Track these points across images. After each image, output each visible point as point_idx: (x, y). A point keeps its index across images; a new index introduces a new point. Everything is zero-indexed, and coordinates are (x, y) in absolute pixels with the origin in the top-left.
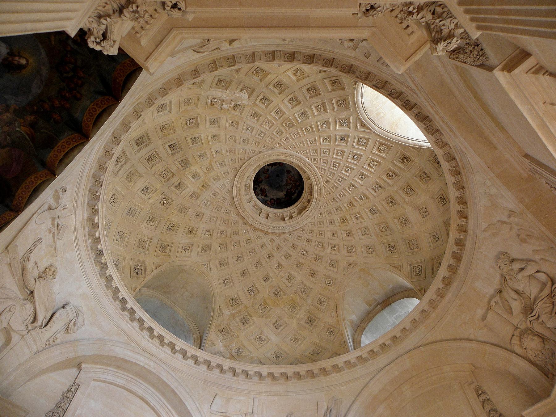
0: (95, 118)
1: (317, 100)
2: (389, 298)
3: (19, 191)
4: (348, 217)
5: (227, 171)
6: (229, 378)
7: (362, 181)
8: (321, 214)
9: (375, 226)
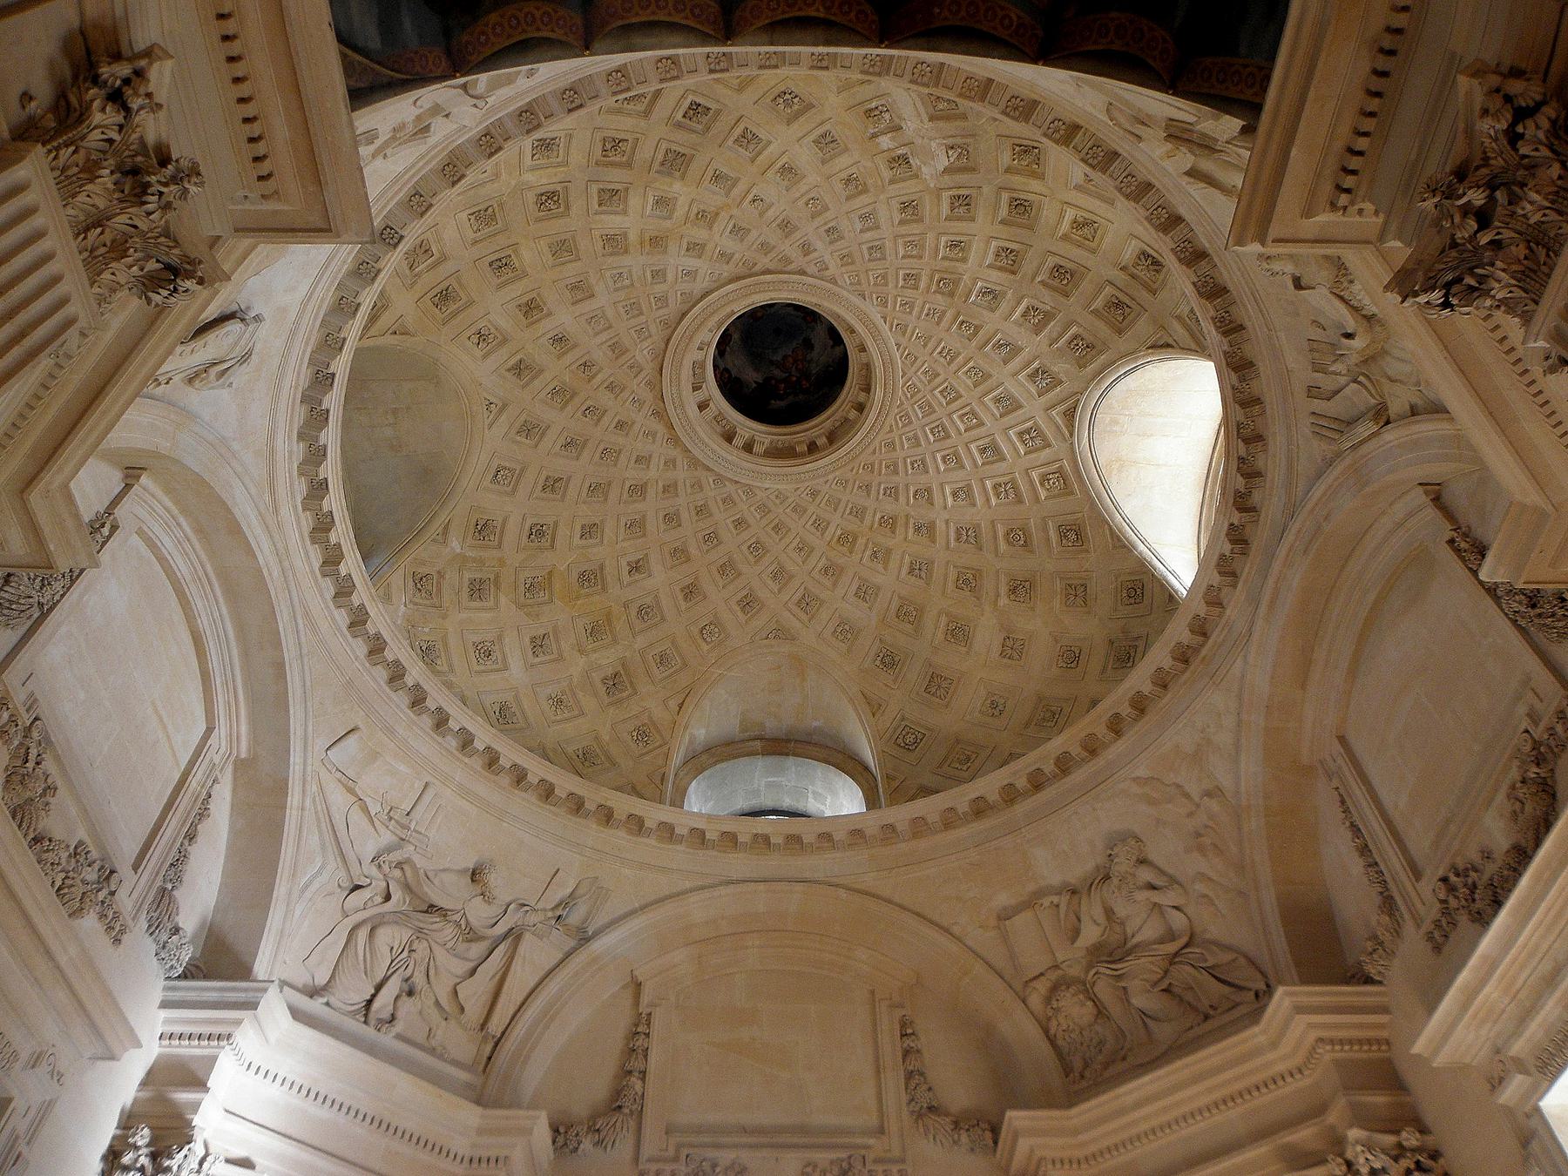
0: (791, 15)
1: (1047, 300)
2: (788, 741)
3: (493, 18)
4: (861, 541)
6: (398, 706)
8: (814, 494)
9: (896, 598)
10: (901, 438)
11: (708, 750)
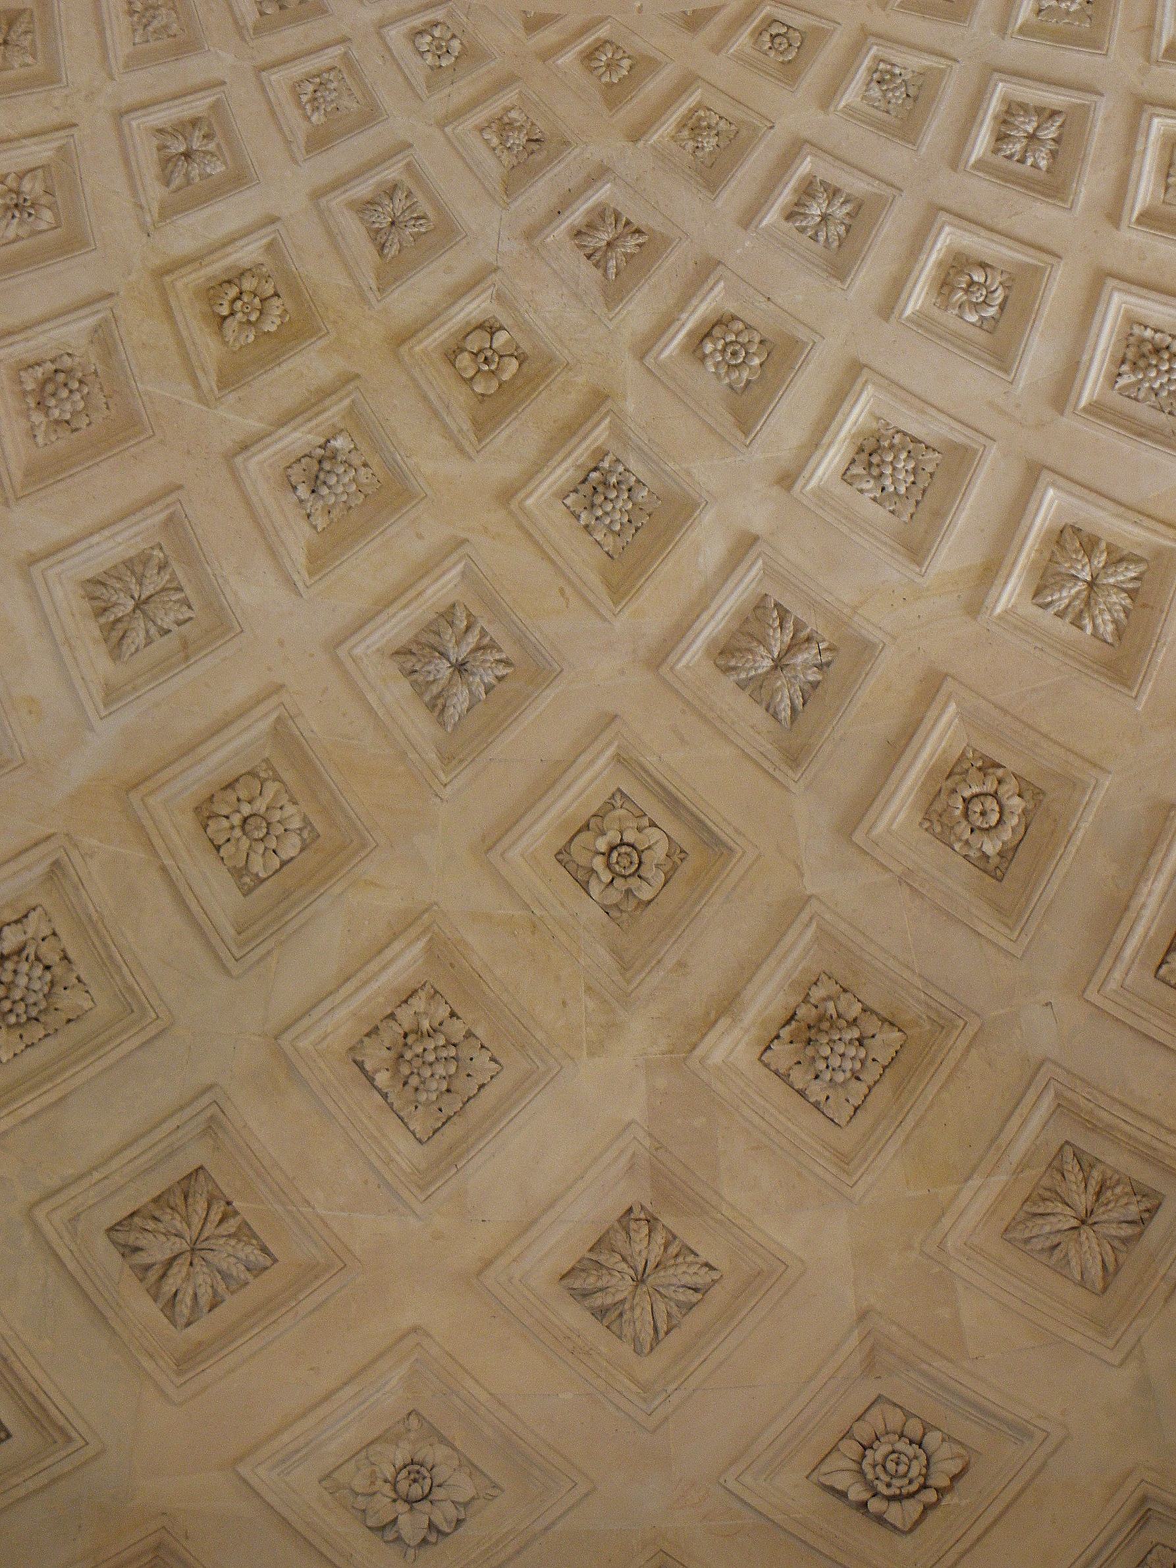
10: (856, 50)
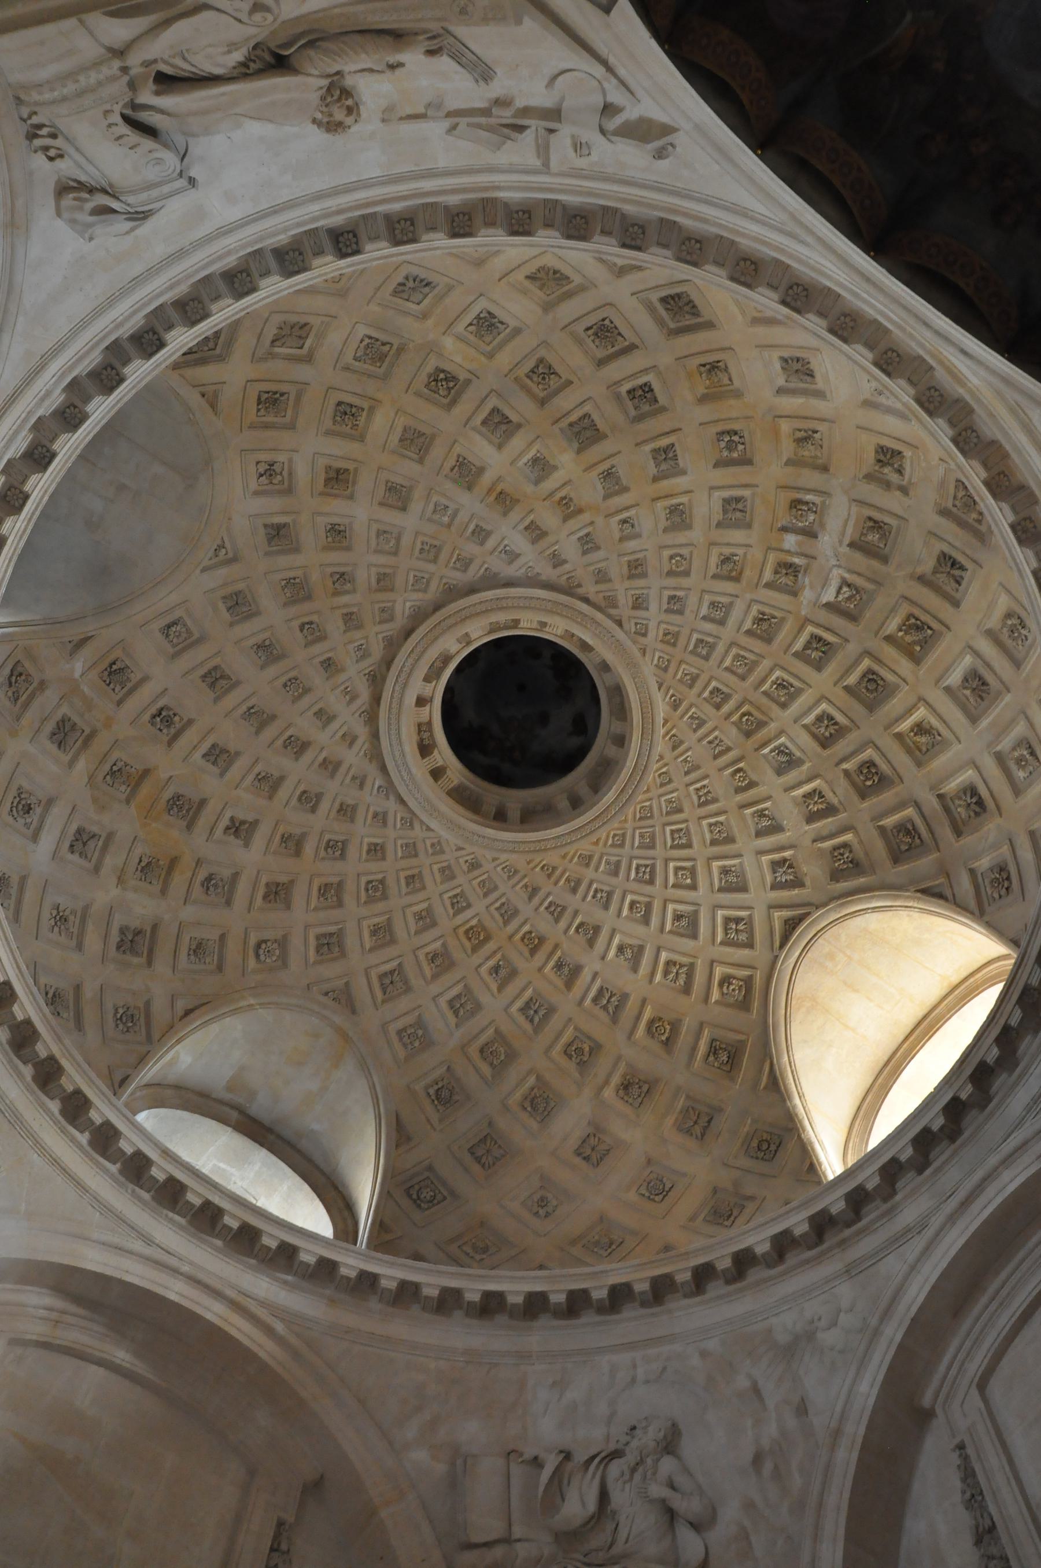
1: (840, 792)
4: (491, 946)
5: (565, 562)
7: (617, 956)
8: (474, 865)
10: (601, 858)
11: (177, 1087)
